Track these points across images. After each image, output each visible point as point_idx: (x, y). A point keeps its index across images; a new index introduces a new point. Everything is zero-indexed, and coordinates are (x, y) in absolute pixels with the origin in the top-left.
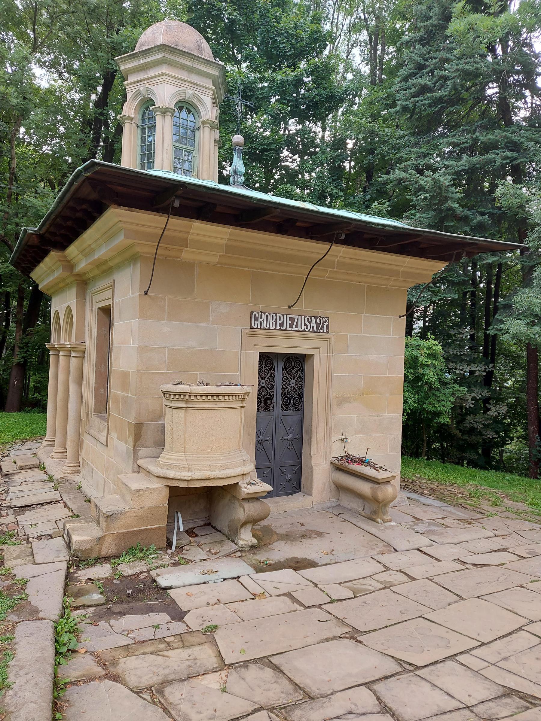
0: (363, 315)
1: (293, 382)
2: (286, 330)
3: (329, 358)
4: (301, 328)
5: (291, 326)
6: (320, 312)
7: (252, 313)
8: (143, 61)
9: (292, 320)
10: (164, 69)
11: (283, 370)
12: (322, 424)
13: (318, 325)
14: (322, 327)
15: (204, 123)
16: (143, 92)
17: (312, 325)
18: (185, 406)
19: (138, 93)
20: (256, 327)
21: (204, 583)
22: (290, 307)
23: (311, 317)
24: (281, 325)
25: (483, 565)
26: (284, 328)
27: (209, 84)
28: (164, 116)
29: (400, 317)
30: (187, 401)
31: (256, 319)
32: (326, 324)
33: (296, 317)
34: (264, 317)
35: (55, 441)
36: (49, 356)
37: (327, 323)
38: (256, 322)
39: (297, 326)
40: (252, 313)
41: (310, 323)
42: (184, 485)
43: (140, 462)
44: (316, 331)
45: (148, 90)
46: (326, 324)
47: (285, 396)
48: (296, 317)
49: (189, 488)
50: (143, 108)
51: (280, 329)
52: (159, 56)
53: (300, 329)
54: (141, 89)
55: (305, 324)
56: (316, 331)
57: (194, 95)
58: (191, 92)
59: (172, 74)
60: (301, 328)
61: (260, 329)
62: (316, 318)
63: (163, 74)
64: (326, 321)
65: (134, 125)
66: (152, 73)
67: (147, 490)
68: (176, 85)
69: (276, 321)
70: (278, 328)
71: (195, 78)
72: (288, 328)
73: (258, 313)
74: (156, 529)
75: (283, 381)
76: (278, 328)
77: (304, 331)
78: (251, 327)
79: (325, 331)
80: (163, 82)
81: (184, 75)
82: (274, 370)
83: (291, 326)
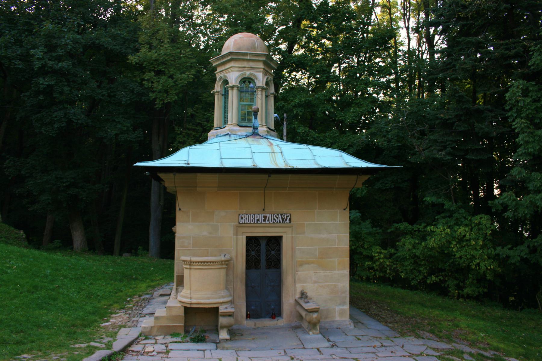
0: (316, 210)
1: (273, 252)
2: (261, 223)
4: (272, 221)
5: (265, 220)
6: (284, 211)
7: (239, 215)
8: (222, 61)
9: (265, 217)
10: (232, 64)
11: (266, 245)
13: (283, 219)
14: (286, 220)
16: (223, 77)
17: (279, 219)
19: (221, 78)
20: (242, 222)
21: (188, 350)
23: (278, 215)
24: (258, 220)
25: (346, 358)
26: (260, 222)
27: (261, 65)
28: (233, 90)
29: (344, 209)
31: (242, 218)
32: (288, 218)
33: (268, 215)
34: (247, 216)
37: (289, 217)
38: (242, 220)
39: (268, 220)
41: (277, 218)
44: (281, 222)
45: (225, 76)
46: (288, 218)
47: (267, 260)
48: (268, 215)
51: (257, 223)
52: (229, 58)
53: (270, 222)
54: (222, 76)
55: (274, 219)
56: (281, 222)
57: (250, 74)
59: (237, 65)
60: (272, 221)
61: (245, 223)
62: (281, 215)
64: (288, 216)
65: (220, 95)
66: (227, 66)
69: (254, 219)
70: (256, 222)
71: (252, 64)
72: (263, 222)
73: (243, 215)
74: (178, 326)
75: (266, 252)
76: (256, 222)
77: (274, 223)
79: (288, 222)
81: (245, 64)
82: (260, 245)
83: (265, 220)
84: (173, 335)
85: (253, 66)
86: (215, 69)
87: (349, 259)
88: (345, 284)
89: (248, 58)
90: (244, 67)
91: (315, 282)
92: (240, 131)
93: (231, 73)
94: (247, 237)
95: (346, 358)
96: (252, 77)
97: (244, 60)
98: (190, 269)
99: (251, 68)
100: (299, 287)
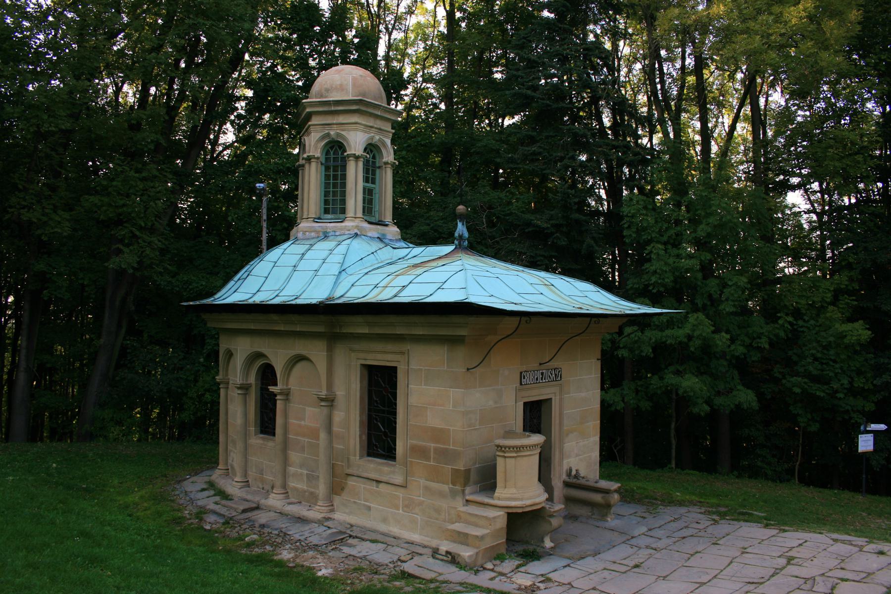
3: (561, 400)
5: (542, 379)
9: (542, 374)
12: (557, 453)
15: (386, 163)
18: (515, 455)
22: (540, 364)
25: (419, 566)
30: (516, 452)
35: (248, 481)
36: (275, 401)
40: (521, 373)
42: (520, 511)
43: (468, 498)
49: (523, 512)
50: (328, 147)
52: (354, 107)
57: (380, 140)
58: (377, 137)
59: (364, 123)
63: (356, 123)
67: (499, 516)
68: (366, 132)
78: (521, 384)
80: (356, 130)
81: (371, 122)
84: (500, 558)
85: (383, 128)
86: (309, 116)
87: (599, 422)
88: (596, 454)
89: (379, 113)
90: (372, 127)
91: (577, 455)
92: (370, 230)
93: (352, 133)
94: (525, 404)
95: (419, 566)
96: (379, 144)
97: (377, 117)
98: (505, 457)
99: (380, 129)
100: (565, 467)
